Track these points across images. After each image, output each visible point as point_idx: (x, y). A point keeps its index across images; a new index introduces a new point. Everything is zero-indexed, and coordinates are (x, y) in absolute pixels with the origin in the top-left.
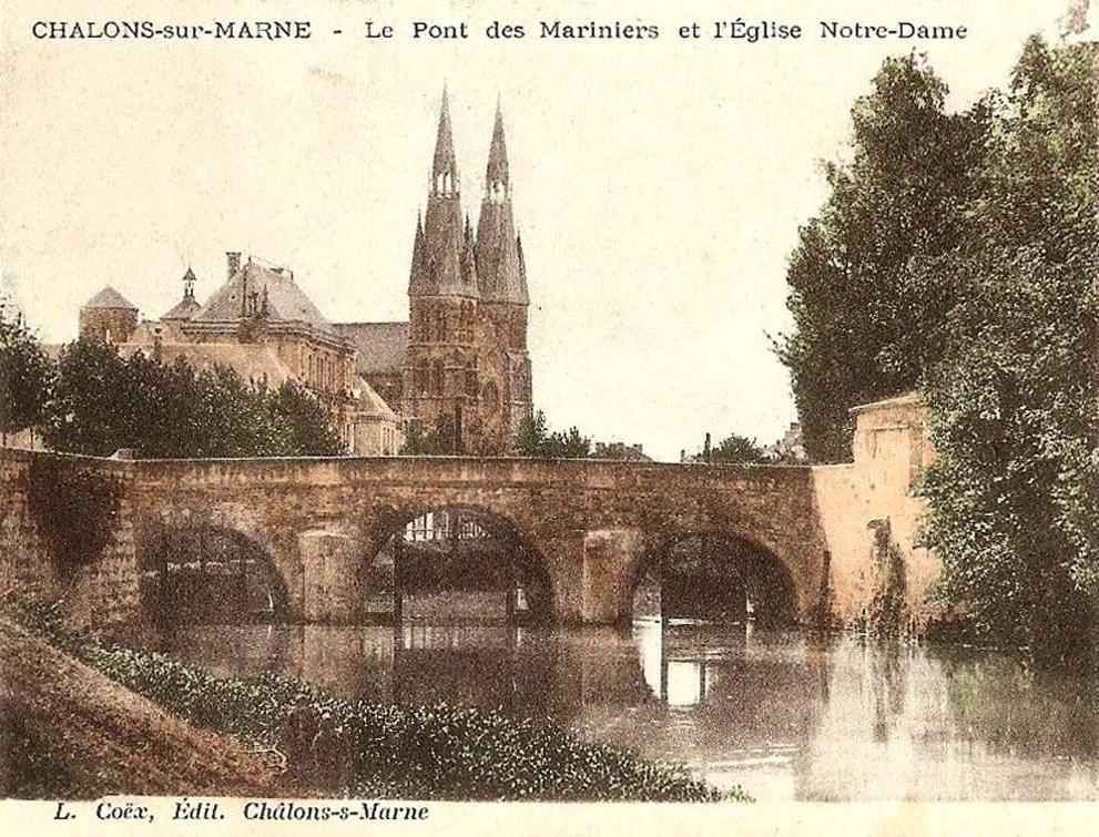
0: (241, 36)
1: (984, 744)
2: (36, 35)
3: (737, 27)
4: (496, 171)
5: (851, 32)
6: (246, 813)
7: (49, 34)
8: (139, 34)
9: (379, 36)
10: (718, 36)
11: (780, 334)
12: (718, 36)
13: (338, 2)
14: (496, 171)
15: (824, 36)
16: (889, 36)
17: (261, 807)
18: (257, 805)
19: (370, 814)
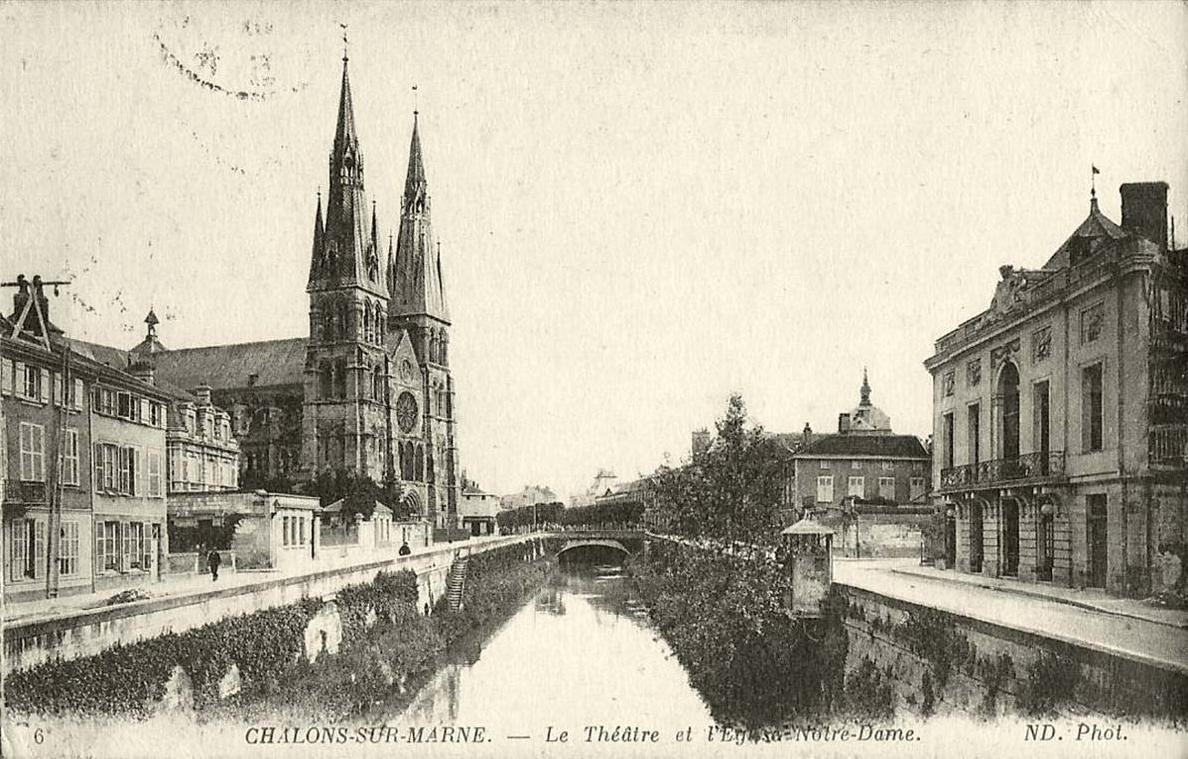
0: (469, 728)
1: (341, 536)
2: (247, 739)
3: (480, 731)
4: (414, 197)
5: (1088, 731)
6: (247, 739)
7: (260, 739)
8: (334, 740)
9: (303, 742)
10: (589, 740)
11: (374, 202)
12: (589, 740)
13: (981, 2)
14: (414, 197)
15: (1027, 739)
16: (851, 738)
17: (261, 732)
18: (257, 731)
19: (457, 463)
